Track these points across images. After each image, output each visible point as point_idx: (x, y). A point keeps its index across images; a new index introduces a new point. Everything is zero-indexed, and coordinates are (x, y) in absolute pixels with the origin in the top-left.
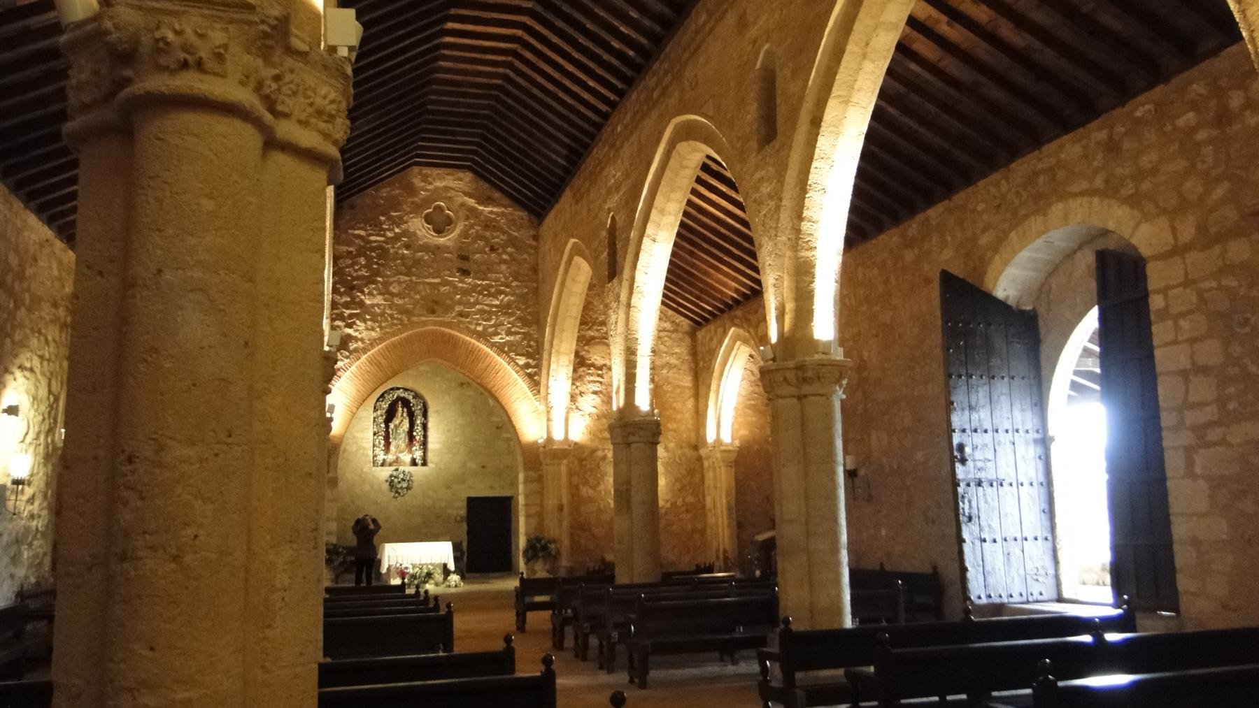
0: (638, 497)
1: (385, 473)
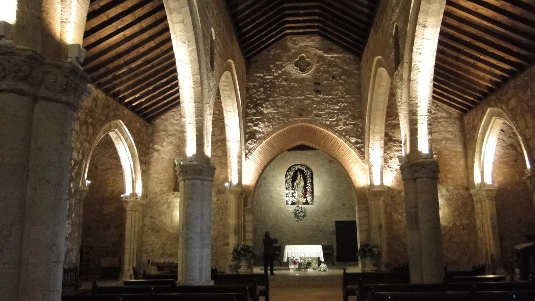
0: (423, 217)
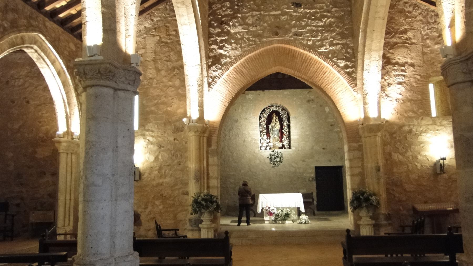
1: (268, 153)
